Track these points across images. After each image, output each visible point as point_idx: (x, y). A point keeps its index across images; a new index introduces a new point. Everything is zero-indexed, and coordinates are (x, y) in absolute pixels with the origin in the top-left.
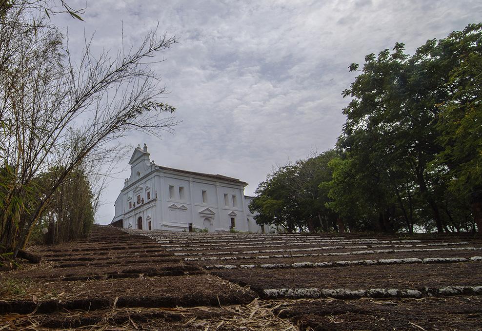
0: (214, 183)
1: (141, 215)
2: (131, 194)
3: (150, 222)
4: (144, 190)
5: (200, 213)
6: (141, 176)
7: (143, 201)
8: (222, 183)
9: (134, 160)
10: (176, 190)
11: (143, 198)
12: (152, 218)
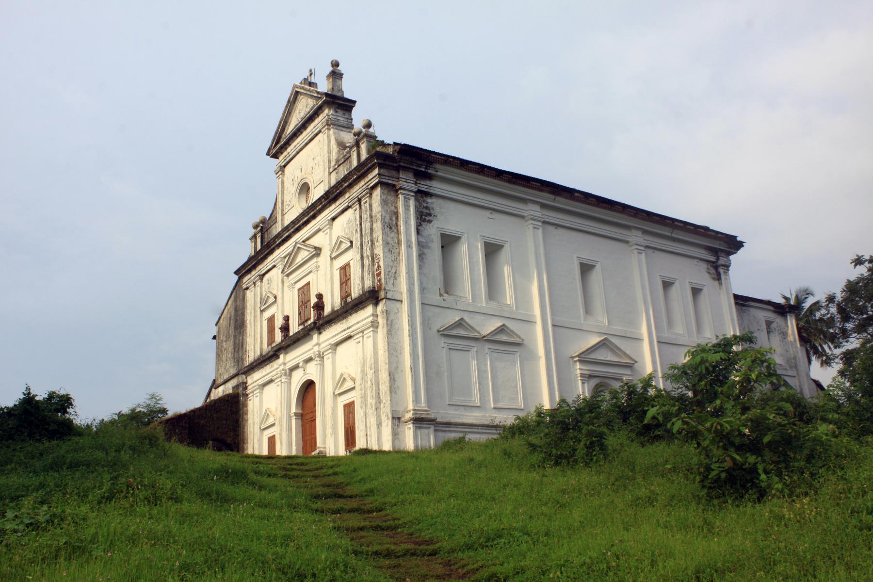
1: (312, 372)
3: (349, 408)
6: (317, 193)
9: (282, 142)
11: (320, 297)
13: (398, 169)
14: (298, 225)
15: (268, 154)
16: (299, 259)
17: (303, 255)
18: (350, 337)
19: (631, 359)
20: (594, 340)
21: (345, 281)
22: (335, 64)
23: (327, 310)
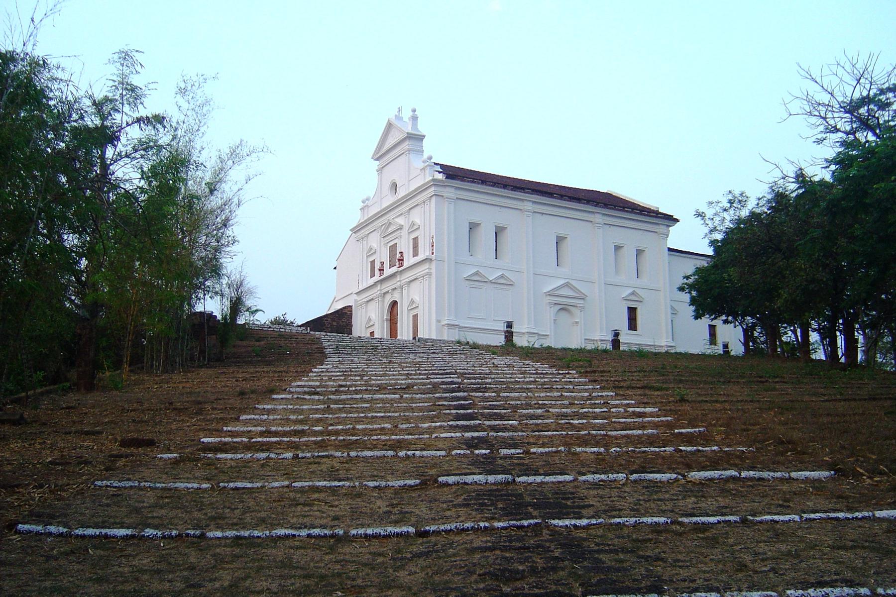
0: (519, 205)
1: (396, 297)
2: (374, 241)
3: (415, 317)
4: (404, 232)
5: (550, 294)
6: (402, 193)
9: (380, 154)
11: (401, 253)
12: (421, 307)
15: (372, 158)
18: (417, 279)
19: (584, 294)
20: (562, 282)
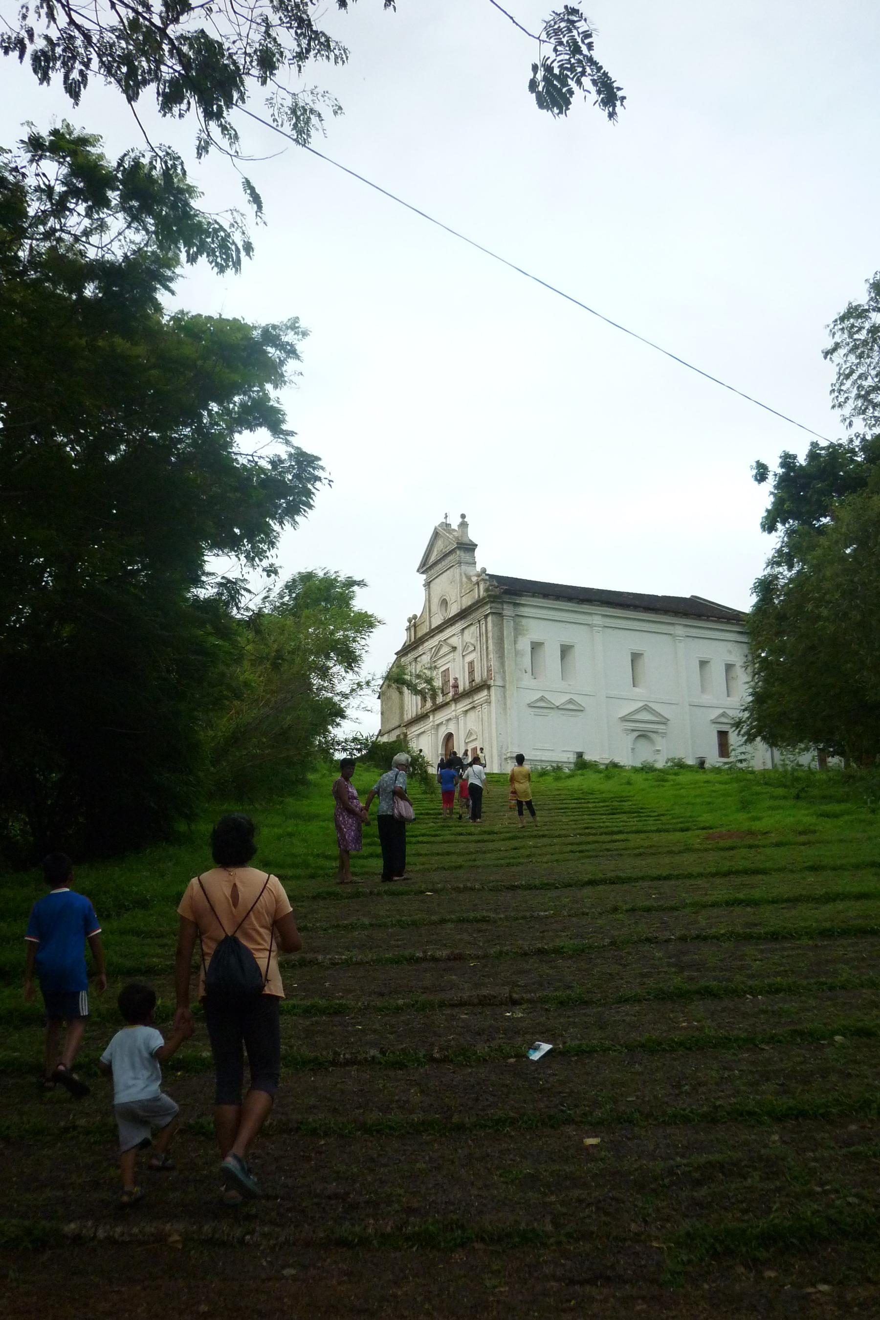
1: (451, 728)
5: (624, 719)
6: (454, 610)
7: (456, 686)
8: (690, 626)
10: (551, 654)
11: (456, 679)
13: (502, 603)
14: (440, 629)
16: (442, 652)
17: (445, 649)
20: (641, 704)
21: (471, 672)
22: (463, 516)
23: (461, 689)
